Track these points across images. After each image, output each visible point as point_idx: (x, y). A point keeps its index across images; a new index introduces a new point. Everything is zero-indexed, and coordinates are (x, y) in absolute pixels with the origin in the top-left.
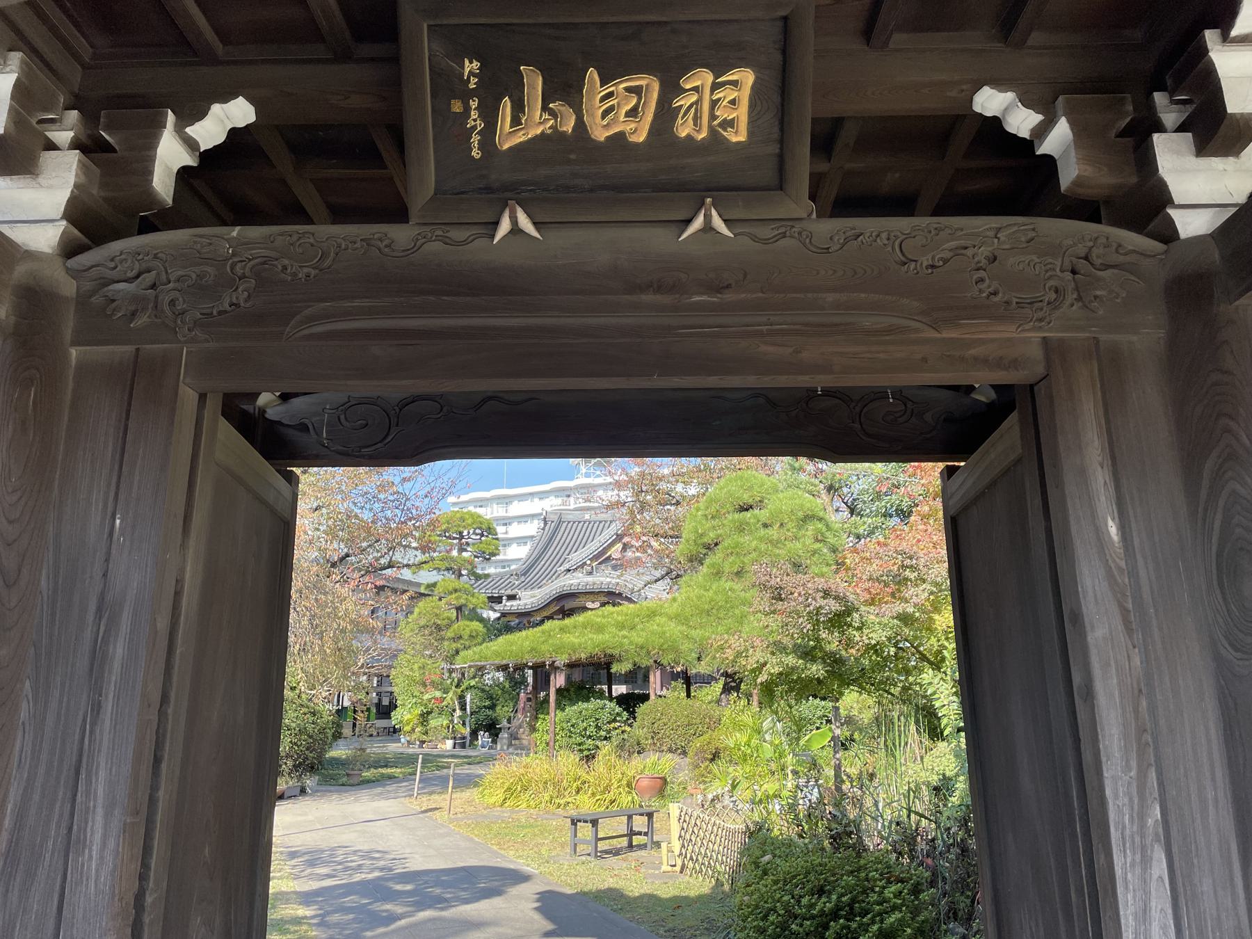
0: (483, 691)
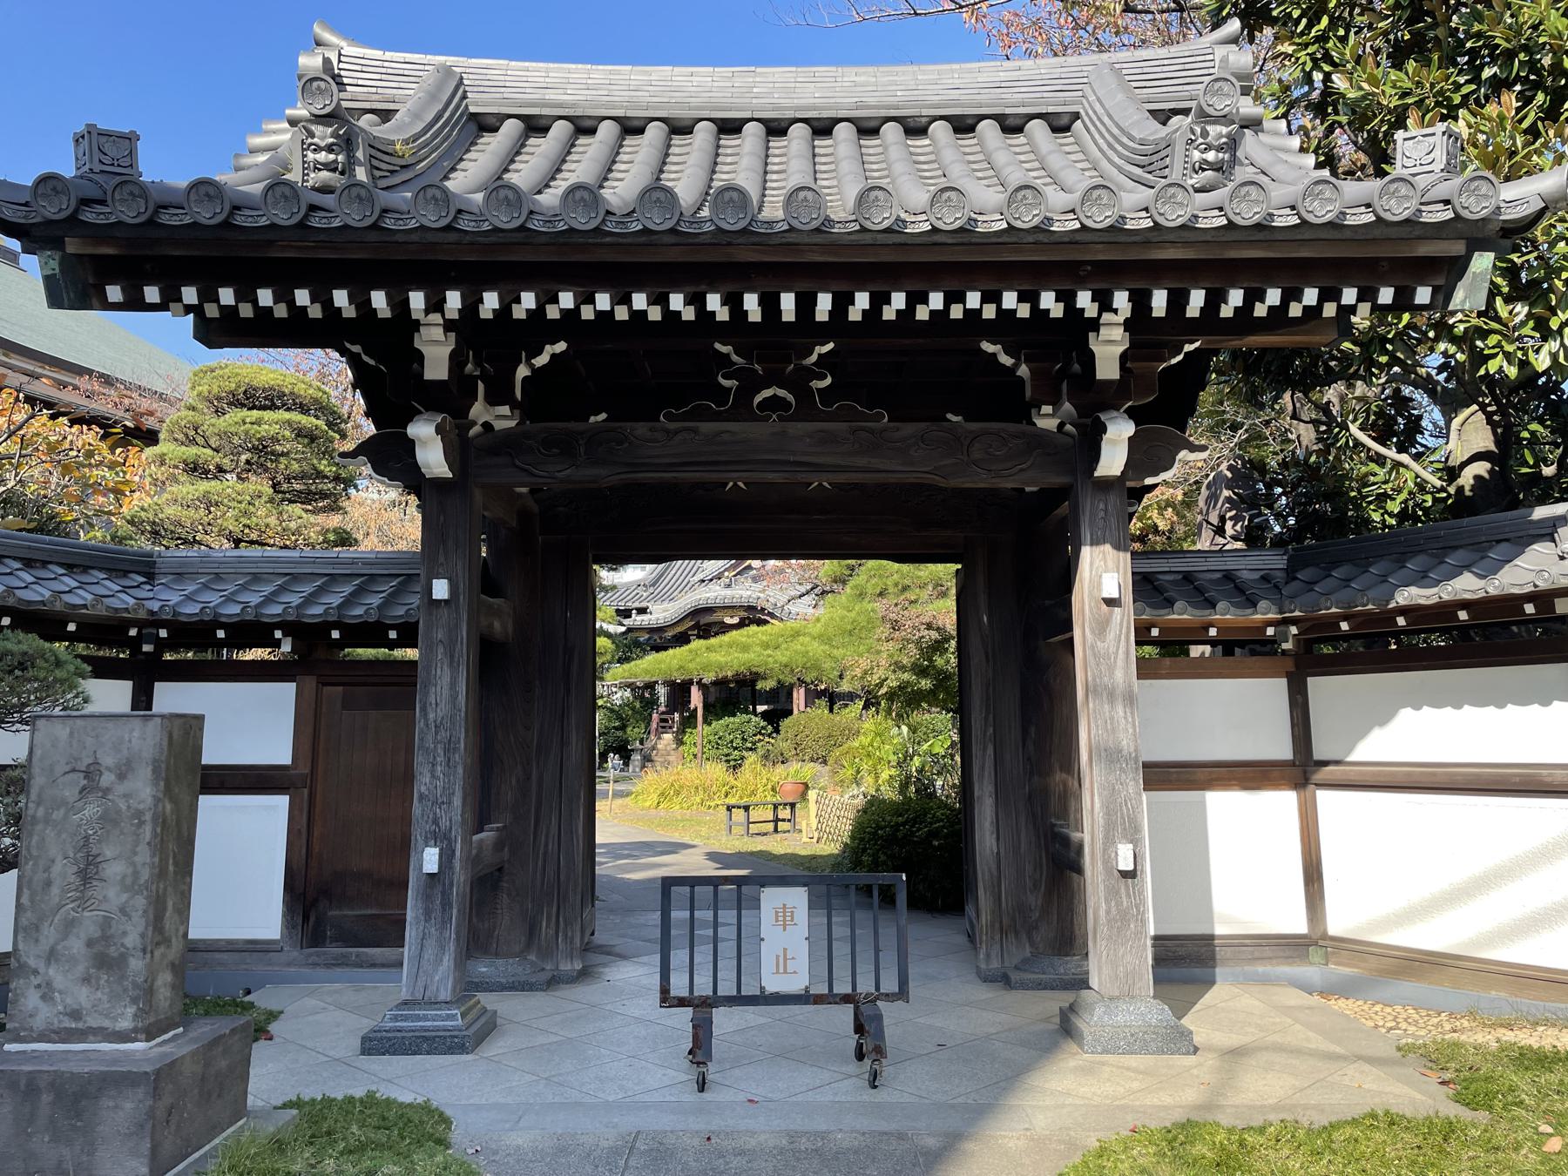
0: (612, 711)
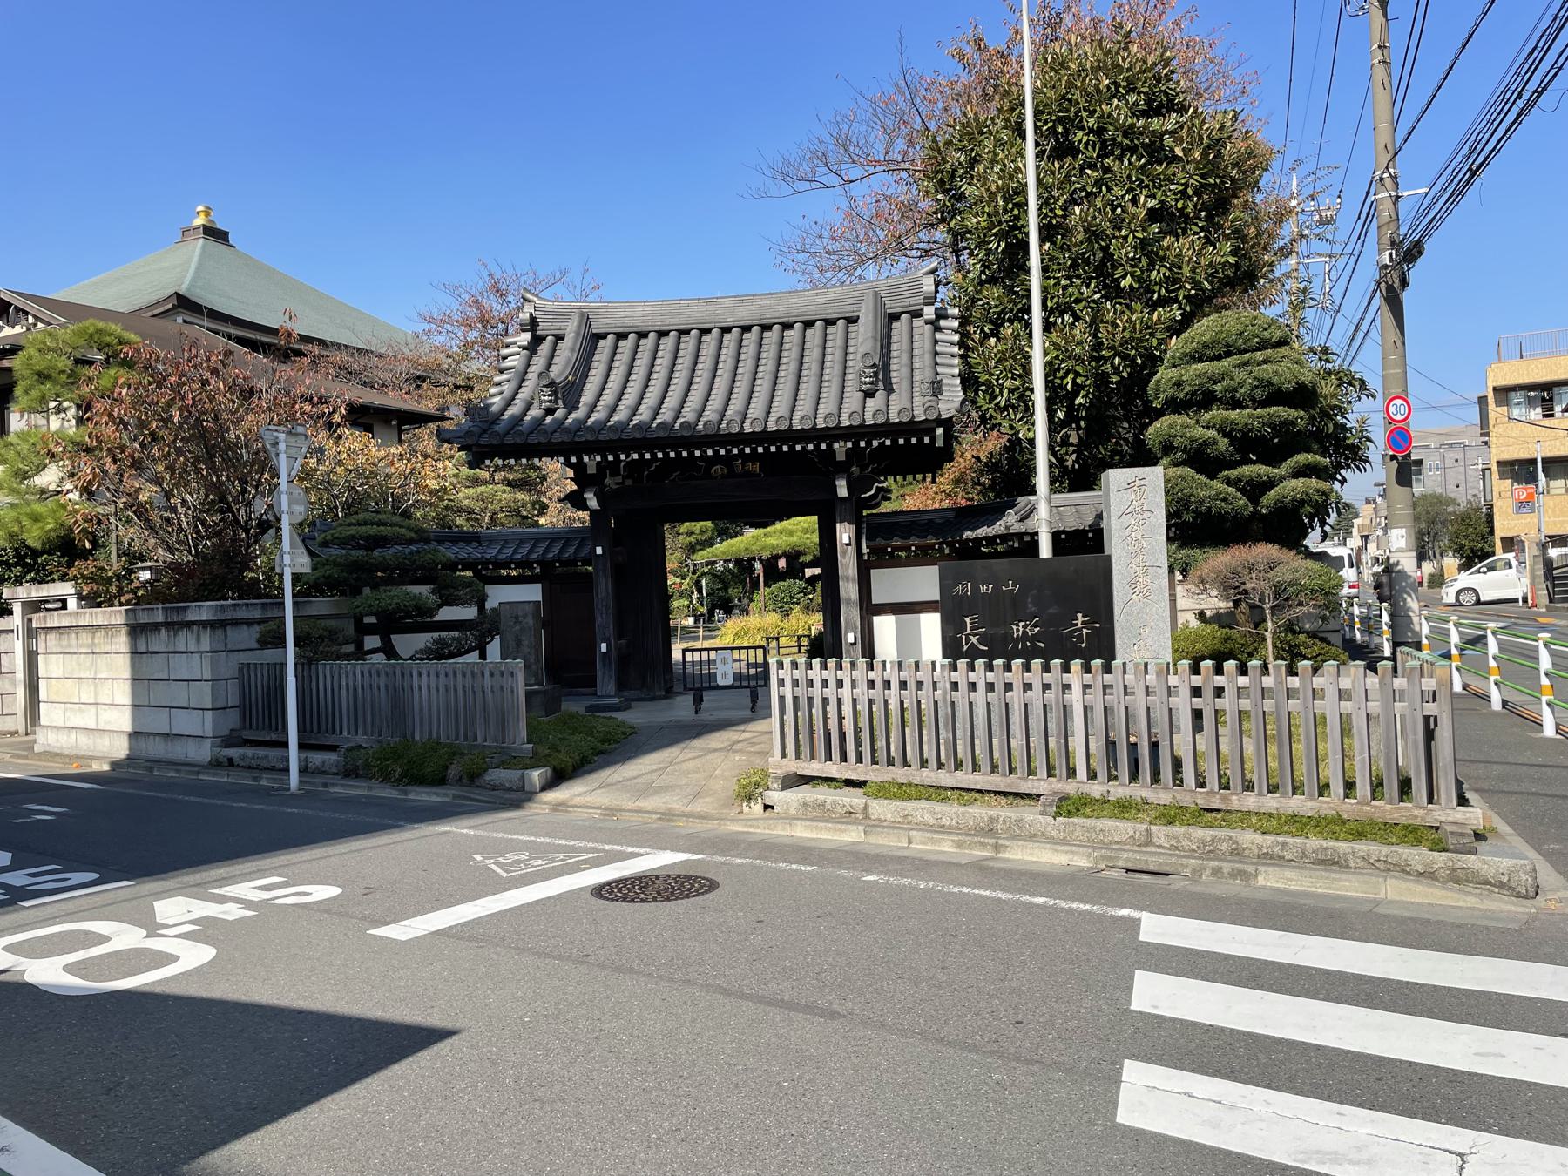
0: (715, 576)
